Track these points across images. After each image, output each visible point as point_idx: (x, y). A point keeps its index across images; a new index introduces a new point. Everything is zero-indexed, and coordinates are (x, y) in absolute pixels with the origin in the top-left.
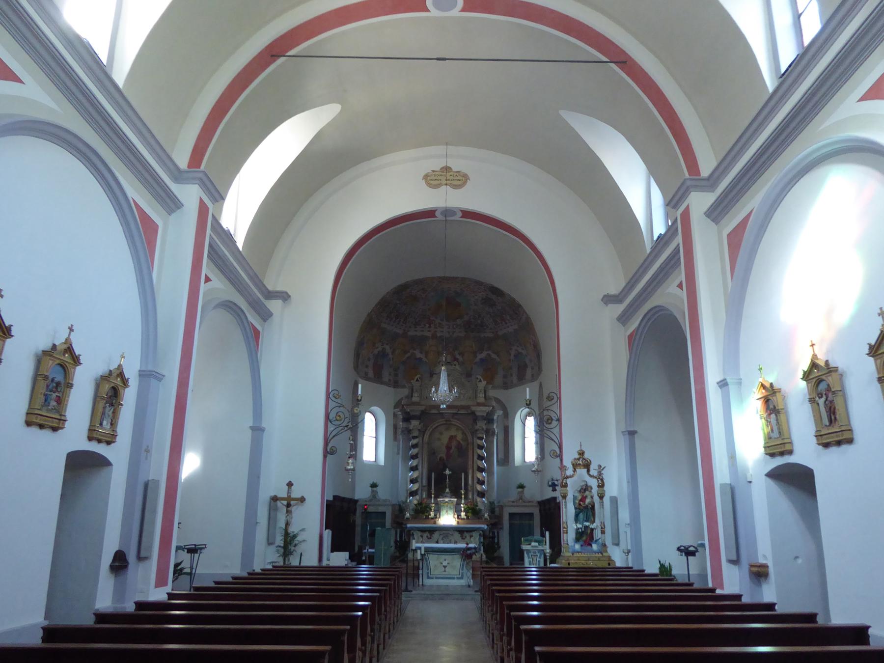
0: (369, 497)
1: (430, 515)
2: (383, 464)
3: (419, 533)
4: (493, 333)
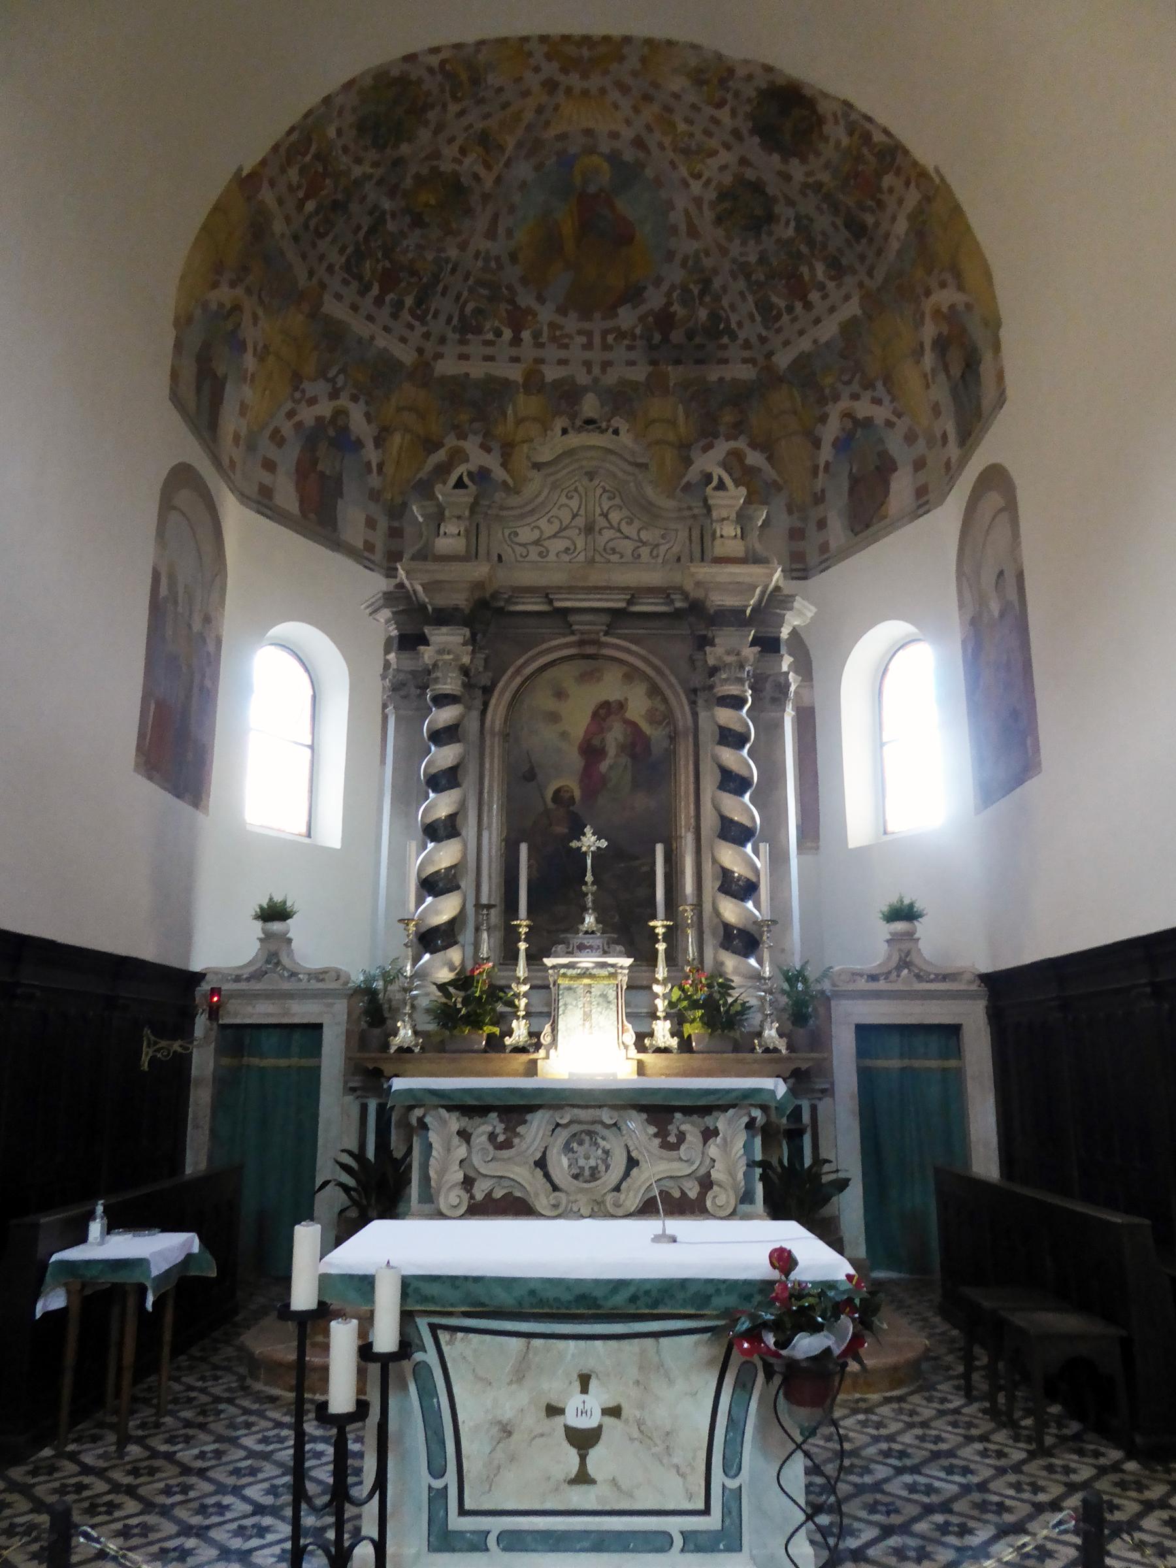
0: (250, 963)
1: (510, 1033)
2: (338, 845)
3: (454, 1122)
4: (752, 361)
